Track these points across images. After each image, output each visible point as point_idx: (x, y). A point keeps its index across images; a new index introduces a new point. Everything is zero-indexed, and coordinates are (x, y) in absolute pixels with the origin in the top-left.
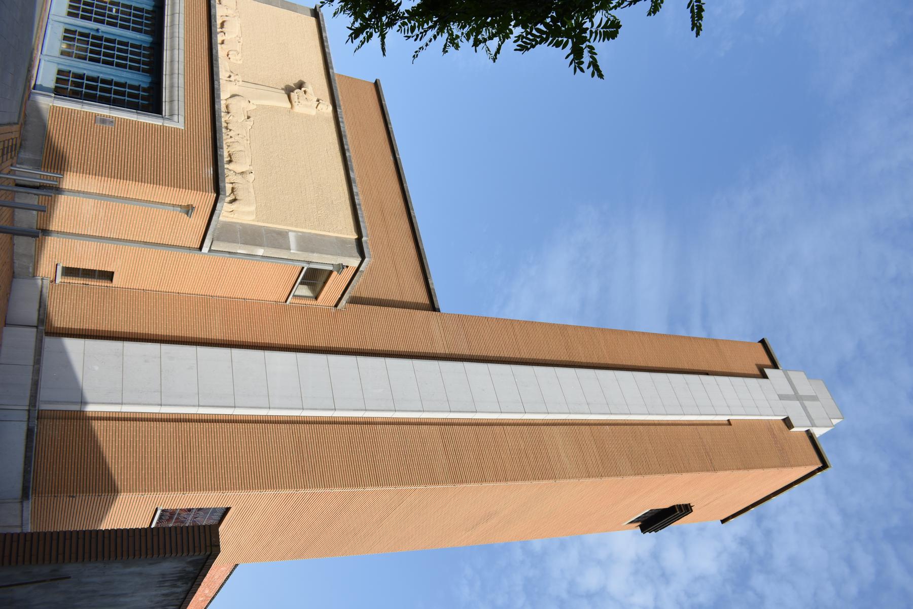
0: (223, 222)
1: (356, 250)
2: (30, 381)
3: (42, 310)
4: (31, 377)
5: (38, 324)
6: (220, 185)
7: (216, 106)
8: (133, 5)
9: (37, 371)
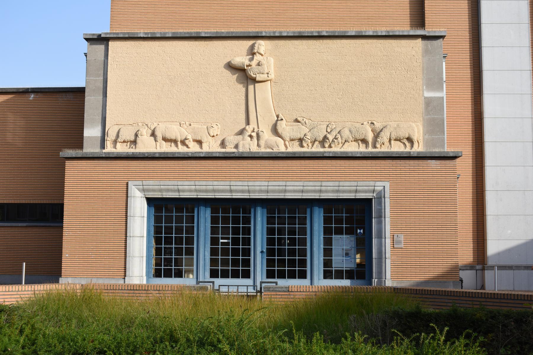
0: (424, 147)
1: (434, 42)
2: (525, 271)
3: (462, 268)
4: (522, 271)
5: (475, 270)
6: (452, 156)
7: (358, 155)
9: (518, 268)
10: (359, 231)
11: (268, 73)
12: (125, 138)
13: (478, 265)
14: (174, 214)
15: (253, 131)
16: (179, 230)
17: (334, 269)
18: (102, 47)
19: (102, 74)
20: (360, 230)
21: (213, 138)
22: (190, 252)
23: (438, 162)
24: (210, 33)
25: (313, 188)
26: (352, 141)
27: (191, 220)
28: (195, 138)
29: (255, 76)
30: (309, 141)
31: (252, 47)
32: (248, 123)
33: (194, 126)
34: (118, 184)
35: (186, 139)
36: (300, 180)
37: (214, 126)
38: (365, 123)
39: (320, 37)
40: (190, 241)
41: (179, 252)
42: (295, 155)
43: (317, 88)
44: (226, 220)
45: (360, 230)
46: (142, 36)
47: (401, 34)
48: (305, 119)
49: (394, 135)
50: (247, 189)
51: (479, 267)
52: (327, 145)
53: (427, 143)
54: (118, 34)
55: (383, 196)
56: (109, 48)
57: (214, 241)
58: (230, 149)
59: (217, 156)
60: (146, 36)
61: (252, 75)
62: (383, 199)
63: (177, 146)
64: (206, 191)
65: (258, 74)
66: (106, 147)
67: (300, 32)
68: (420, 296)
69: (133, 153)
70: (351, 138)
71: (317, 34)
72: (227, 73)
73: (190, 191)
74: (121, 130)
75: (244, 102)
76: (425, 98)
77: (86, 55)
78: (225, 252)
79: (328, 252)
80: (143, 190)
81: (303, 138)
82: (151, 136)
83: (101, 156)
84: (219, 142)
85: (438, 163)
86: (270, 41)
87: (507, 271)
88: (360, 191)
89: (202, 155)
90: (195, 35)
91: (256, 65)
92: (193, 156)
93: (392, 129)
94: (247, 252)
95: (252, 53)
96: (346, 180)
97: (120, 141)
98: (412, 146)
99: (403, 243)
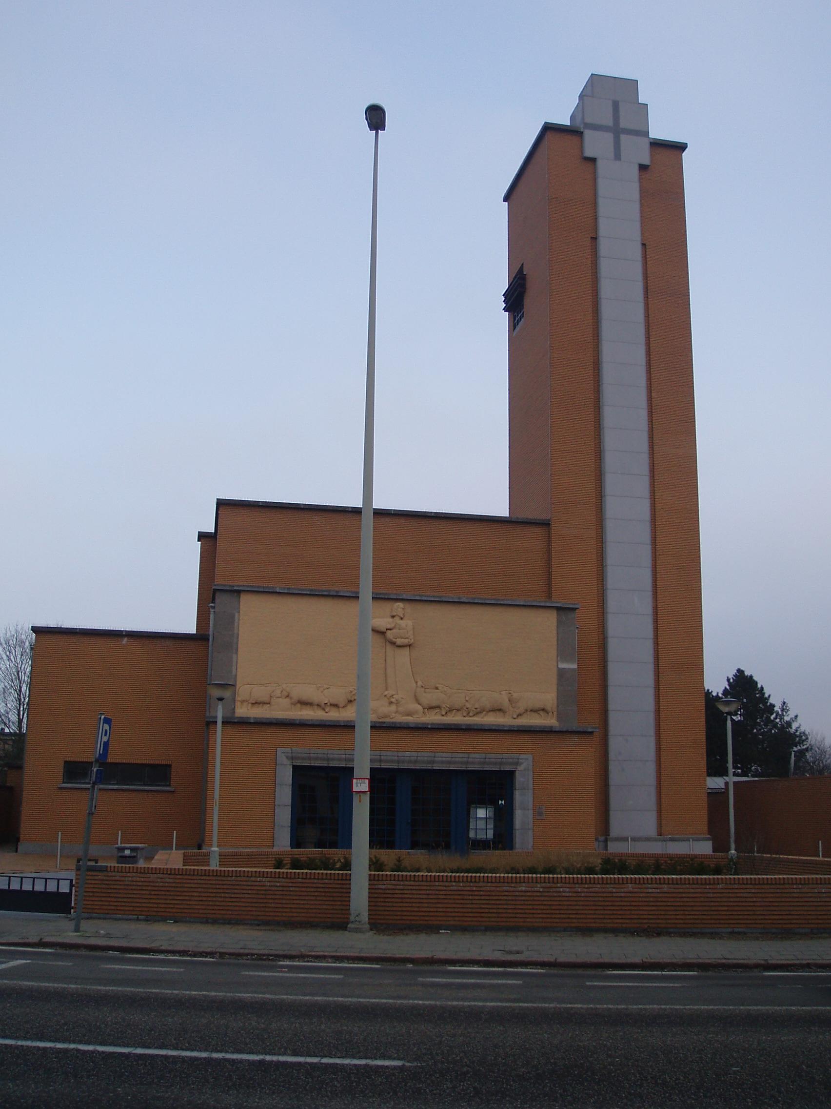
25: (460, 760)
68: (271, 879)
71: (335, 594)
80: (292, 758)
99: (544, 815)
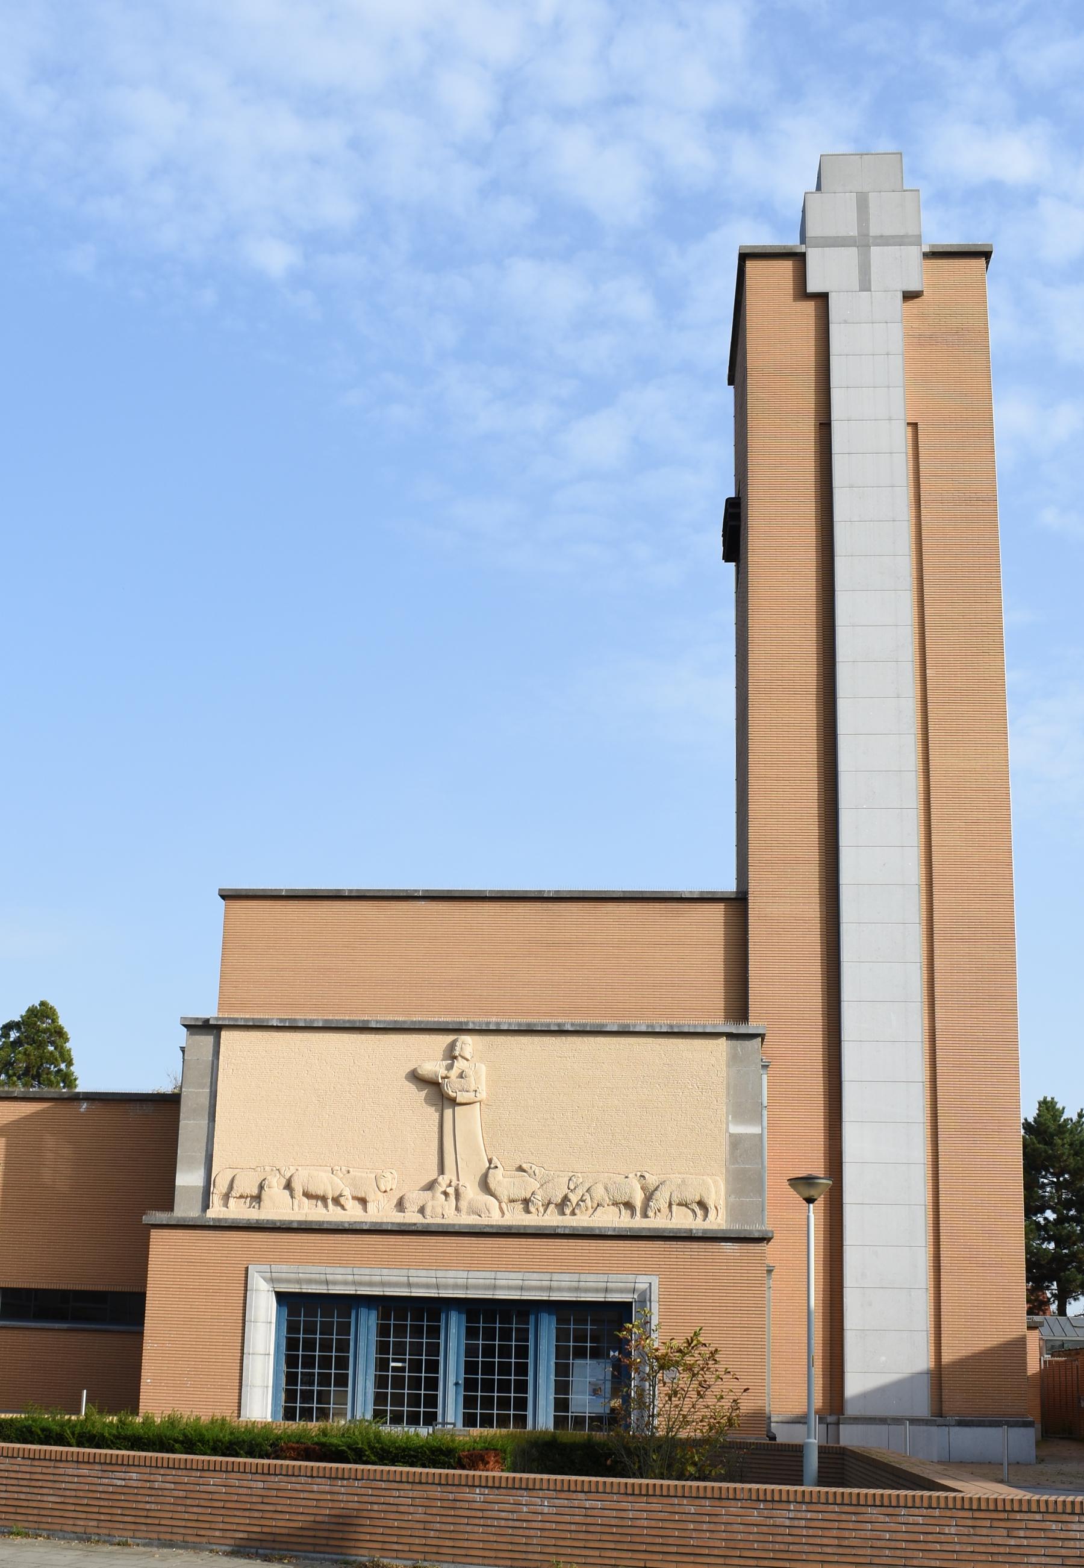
8: (529, 1344)
10: (612, 1353)
11: (476, 1091)
12: (242, 1191)
13: (830, 1415)
14: (319, 1319)
15: (450, 1185)
16: (326, 1346)
17: (570, 1414)
18: (209, 1039)
19: (209, 1084)
20: (614, 1352)
21: (385, 1194)
22: (342, 1381)
23: (736, 1246)
24: (385, 1022)
25: (538, 1283)
26: (608, 1205)
27: (345, 1329)
28: (355, 1194)
29: (454, 1095)
30: (540, 1203)
31: (452, 1046)
32: (442, 1171)
33: (354, 1173)
34: (232, 1269)
35: (341, 1195)
36: (518, 1270)
37: (388, 1175)
38: (630, 1176)
39: (561, 1032)
40: (343, 1363)
41: (325, 1380)
42: (511, 1230)
43: (555, 1117)
44: (400, 1331)
45: (614, 1352)
46: (275, 1025)
47: (692, 1030)
48: (534, 1167)
49: (677, 1197)
50: (435, 1282)
51: (831, 1419)
52: (568, 1211)
53: (733, 1211)
54: (236, 1019)
55: (648, 1297)
56: (221, 1041)
57: (382, 1365)
58: (411, 1217)
59: (389, 1228)
60: (282, 1025)
61: (451, 1093)
62: (648, 1303)
63: (326, 1206)
64: (371, 1284)
65: (460, 1091)
66: (211, 1205)
67: (529, 1024)
69: (257, 1220)
70: (608, 1200)
71: (556, 1028)
72: (411, 1088)
73: (346, 1283)
74: (237, 1177)
75: (436, 1136)
76: (731, 1135)
77: (183, 1049)
78: (398, 1382)
79: (562, 1387)
80: (272, 1280)
81: (530, 1198)
82: (285, 1188)
83: (207, 1224)
84: (395, 1202)
85: (736, 1248)
86: (481, 1037)
87: (878, 1427)
88: (612, 1291)
89: (365, 1227)
90: (361, 1025)
91: (457, 1077)
92: (351, 1227)
93: (674, 1188)
94: (433, 1384)
95: (451, 1055)
96: (590, 1272)
97: (234, 1195)
98: (706, 1216)
